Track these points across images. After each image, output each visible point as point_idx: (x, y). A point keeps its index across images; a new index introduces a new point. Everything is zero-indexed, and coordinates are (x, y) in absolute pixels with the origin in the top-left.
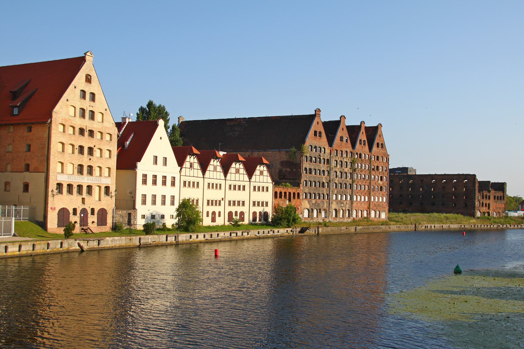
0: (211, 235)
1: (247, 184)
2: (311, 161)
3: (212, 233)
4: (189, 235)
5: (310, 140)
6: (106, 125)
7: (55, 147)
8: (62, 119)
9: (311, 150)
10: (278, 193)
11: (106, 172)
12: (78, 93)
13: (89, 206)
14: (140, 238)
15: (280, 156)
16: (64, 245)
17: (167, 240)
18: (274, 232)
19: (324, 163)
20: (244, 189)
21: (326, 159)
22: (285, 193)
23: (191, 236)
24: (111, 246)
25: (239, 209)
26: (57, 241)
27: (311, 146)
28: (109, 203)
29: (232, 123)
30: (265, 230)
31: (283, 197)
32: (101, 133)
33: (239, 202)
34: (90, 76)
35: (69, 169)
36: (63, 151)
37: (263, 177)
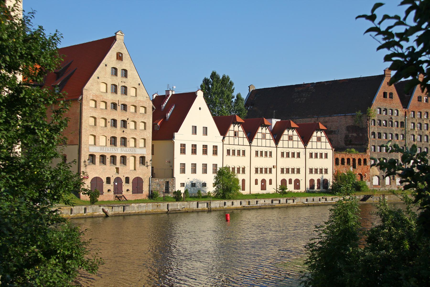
0: (249, 202)
1: (302, 151)
2: (380, 124)
3: (250, 200)
4: (223, 202)
5: (378, 102)
6: (141, 99)
8: (93, 96)
9: (380, 113)
11: (141, 143)
12: (109, 70)
13: (123, 175)
14: (168, 205)
15: (342, 121)
16: (87, 211)
17: (197, 207)
18: (326, 200)
19: (397, 126)
20: (271, 155)
21: (399, 121)
22: (348, 160)
23: (225, 203)
24: (137, 211)
25: (294, 177)
26: (80, 207)
27: (380, 109)
28: (144, 173)
29: (300, 89)
30: (315, 198)
31: (346, 163)
32: (135, 106)
33: (266, 169)
34: (122, 54)
35: (102, 141)
36: (95, 124)
37: (320, 143)
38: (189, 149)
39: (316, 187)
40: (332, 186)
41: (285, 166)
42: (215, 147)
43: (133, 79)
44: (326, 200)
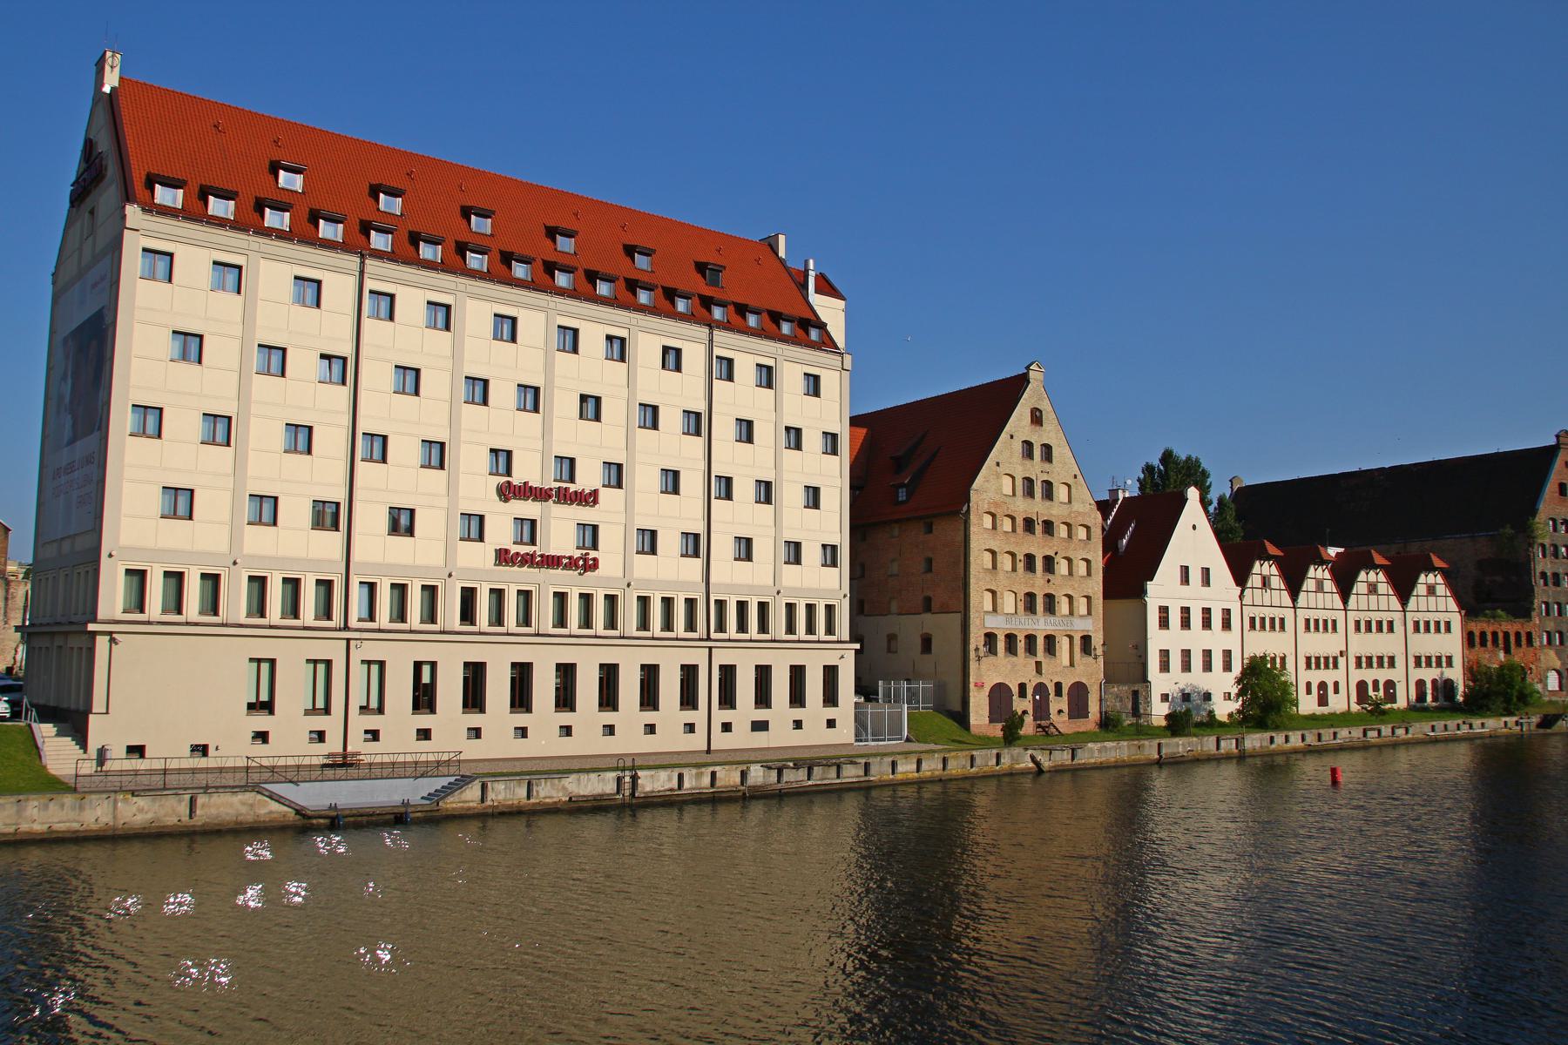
1: (1397, 618)
4: (1267, 735)
6: (1077, 507)
7: (979, 560)
9: (1555, 529)
10: (1477, 634)
12: (1018, 447)
17: (1218, 748)
22: (1495, 634)
25: (1383, 675)
27: (1554, 520)
28: (1091, 672)
31: (1489, 644)
37: (1435, 598)
38: (1175, 618)
39: (1429, 698)
40: (1465, 695)
41: (1365, 652)
42: (1227, 612)
43: (1064, 466)
44: (1471, 727)
